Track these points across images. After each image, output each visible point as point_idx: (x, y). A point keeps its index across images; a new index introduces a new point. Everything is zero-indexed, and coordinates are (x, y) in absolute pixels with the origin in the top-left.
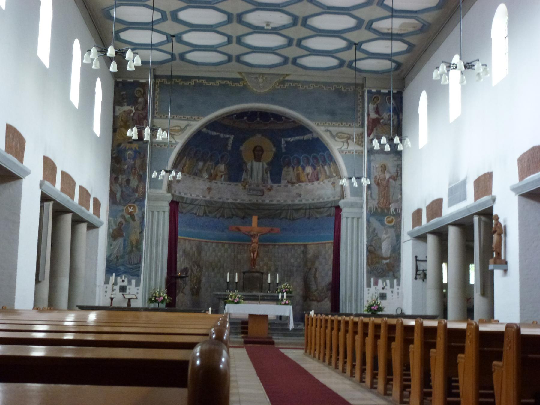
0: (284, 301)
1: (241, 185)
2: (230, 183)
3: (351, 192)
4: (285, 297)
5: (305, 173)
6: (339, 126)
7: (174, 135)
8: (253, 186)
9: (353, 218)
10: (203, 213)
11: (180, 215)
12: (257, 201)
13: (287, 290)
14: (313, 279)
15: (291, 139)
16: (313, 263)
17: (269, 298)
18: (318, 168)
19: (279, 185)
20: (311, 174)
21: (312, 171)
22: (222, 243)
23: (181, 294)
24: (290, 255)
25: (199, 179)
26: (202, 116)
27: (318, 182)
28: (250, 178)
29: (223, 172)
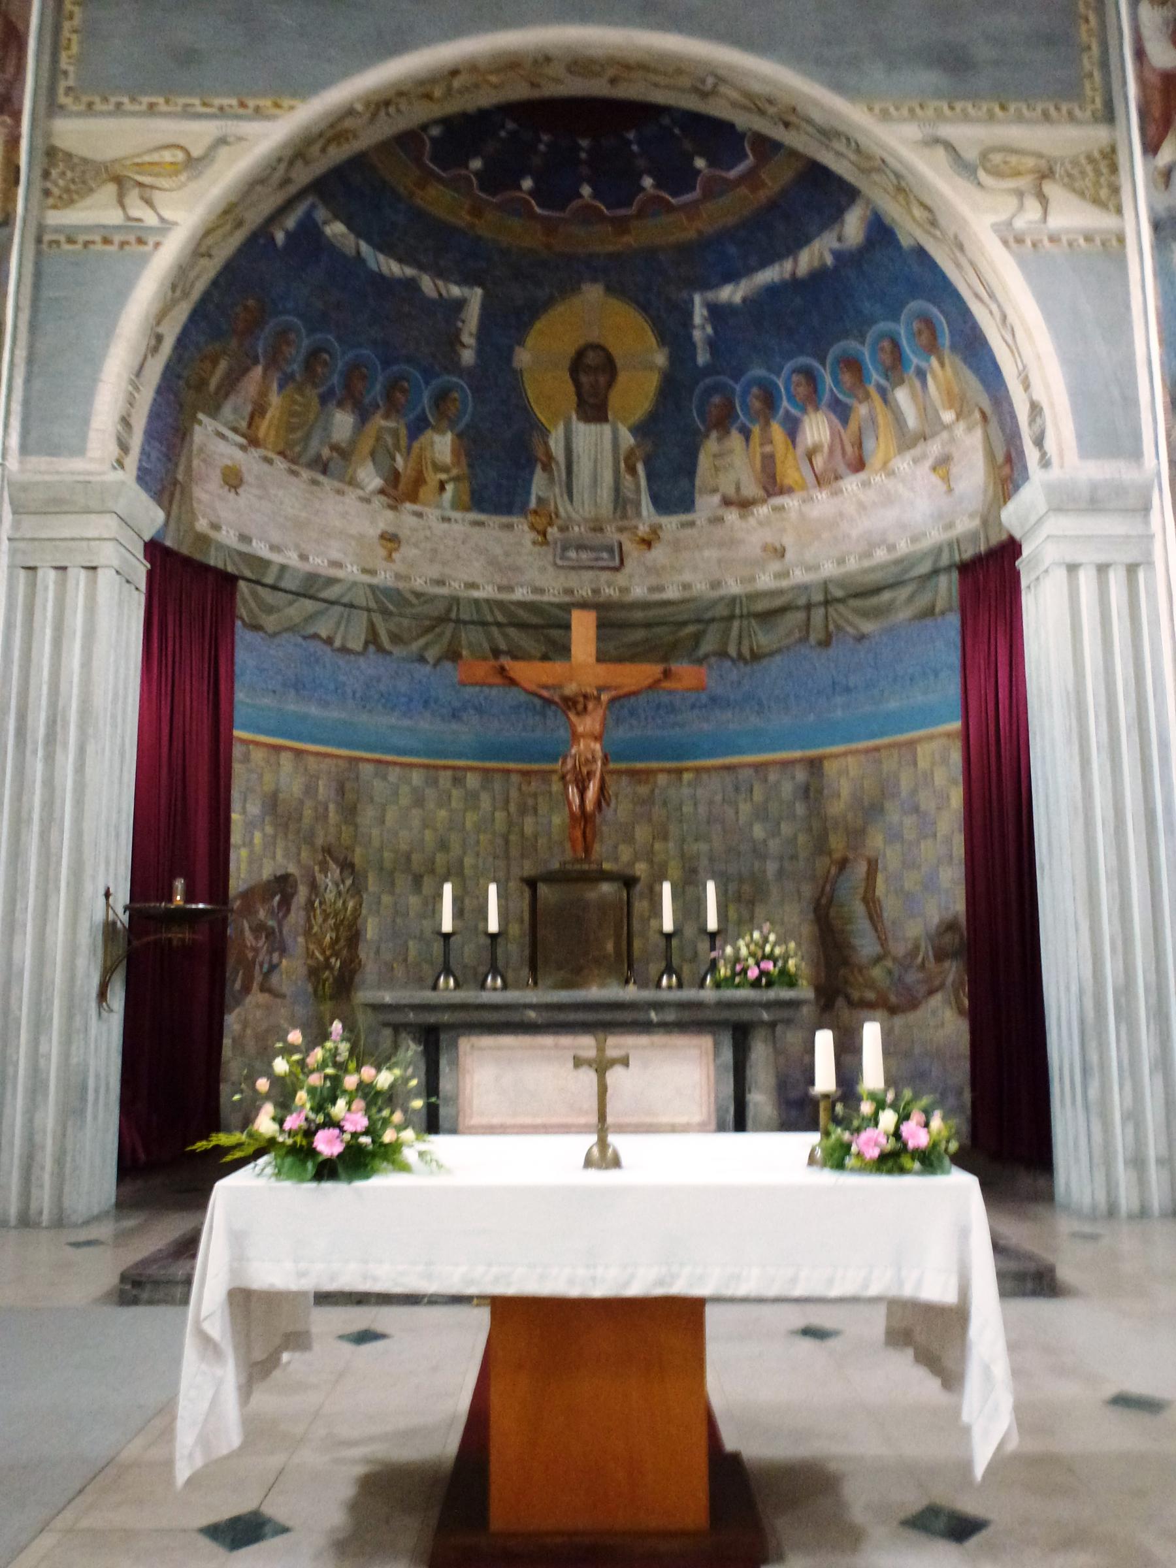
0: (874, 1120)
1: (526, 528)
2: (482, 517)
3: (1080, 437)
4: (873, 1075)
5: (800, 450)
6: (991, 118)
7: (152, 187)
8: (576, 529)
9: (1102, 569)
10: (363, 638)
11: (244, 638)
12: (596, 591)
13: (769, 966)
14: (859, 908)
15: (733, 293)
16: (856, 835)
17: (671, 1016)
18: (862, 410)
19: (684, 517)
20: (826, 449)
21: (831, 428)
22: (454, 768)
23: (256, 997)
24: (745, 808)
25: (340, 492)
26: (295, 94)
27: (862, 476)
28: (566, 497)
29: (445, 469)
